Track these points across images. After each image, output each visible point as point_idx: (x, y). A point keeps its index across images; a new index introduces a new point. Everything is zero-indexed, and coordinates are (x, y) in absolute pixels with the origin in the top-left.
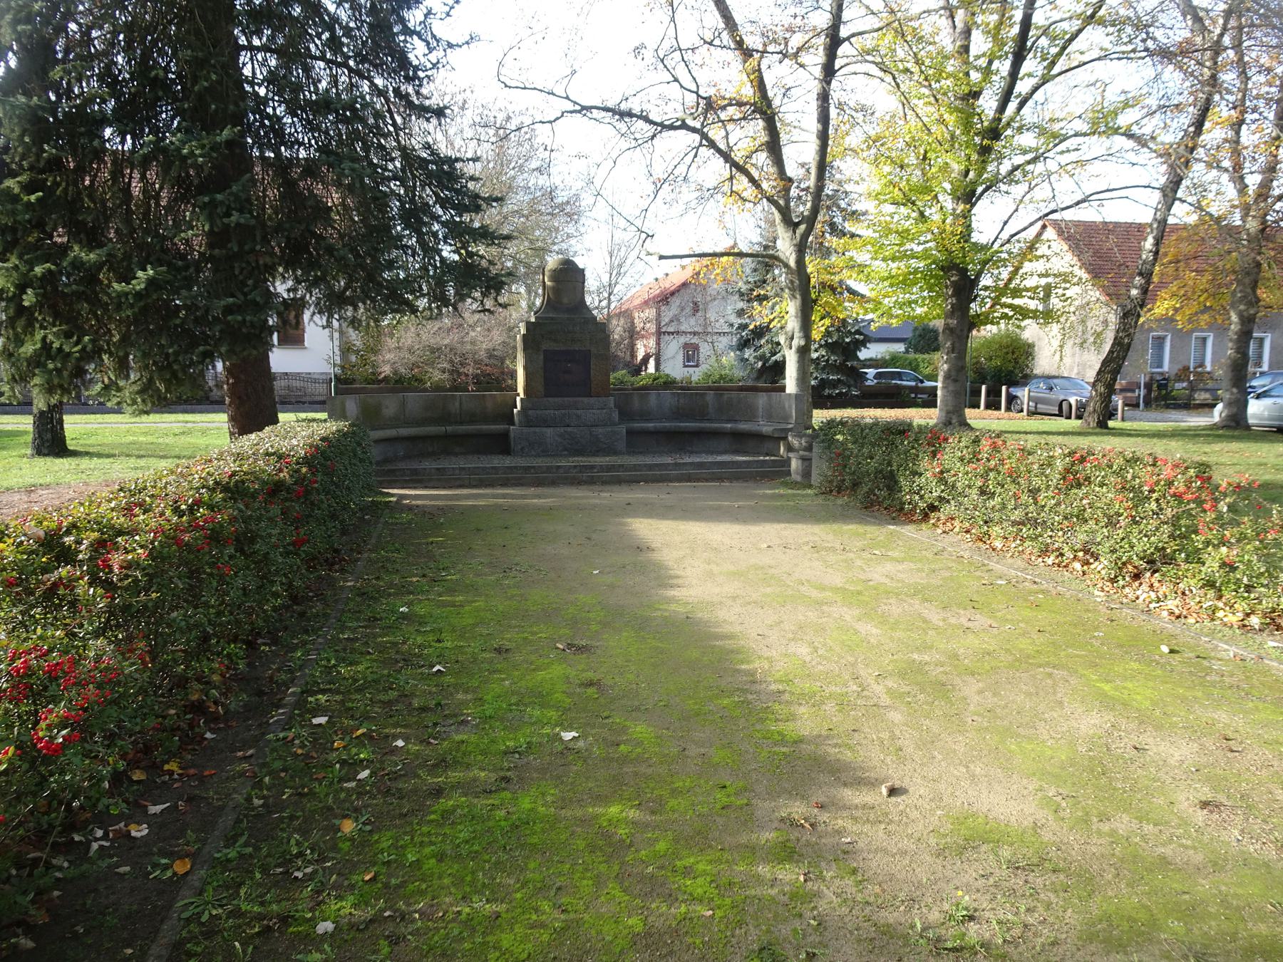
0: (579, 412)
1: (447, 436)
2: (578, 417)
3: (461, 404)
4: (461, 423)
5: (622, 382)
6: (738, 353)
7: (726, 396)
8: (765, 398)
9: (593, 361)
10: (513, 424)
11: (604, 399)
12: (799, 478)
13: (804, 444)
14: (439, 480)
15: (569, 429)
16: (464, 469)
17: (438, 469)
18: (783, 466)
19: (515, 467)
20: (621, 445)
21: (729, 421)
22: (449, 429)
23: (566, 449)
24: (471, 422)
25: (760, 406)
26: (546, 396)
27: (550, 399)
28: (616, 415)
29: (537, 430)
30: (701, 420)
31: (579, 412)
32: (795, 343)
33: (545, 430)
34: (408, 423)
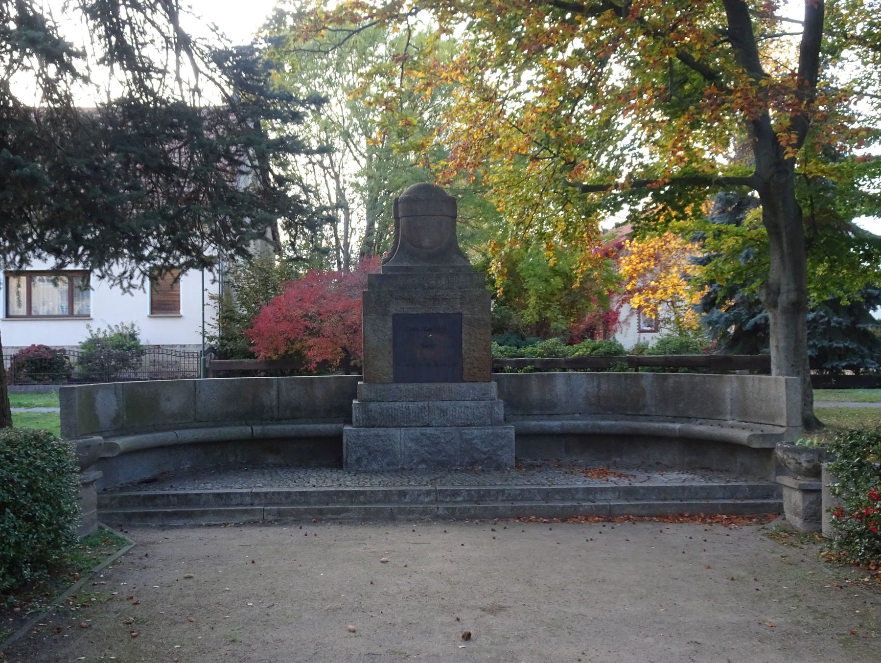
0: (444, 404)
1: (252, 441)
2: (443, 412)
3: (278, 394)
4: (279, 420)
5: (553, 353)
6: (704, 314)
7: (671, 381)
8: (735, 384)
9: (465, 329)
10: (349, 422)
11: (483, 385)
12: (798, 522)
13: (805, 464)
14: (217, 513)
15: (429, 431)
16: (257, 494)
17: (218, 495)
18: (768, 496)
19: (337, 493)
20: (508, 456)
21: (675, 419)
22: (258, 429)
23: (423, 461)
24: (293, 419)
25: (728, 396)
26: (396, 381)
27: (402, 386)
28: (500, 410)
29: (381, 431)
30: (635, 416)
31: (444, 404)
32: (783, 300)
33: (393, 431)
34: (200, 422)
